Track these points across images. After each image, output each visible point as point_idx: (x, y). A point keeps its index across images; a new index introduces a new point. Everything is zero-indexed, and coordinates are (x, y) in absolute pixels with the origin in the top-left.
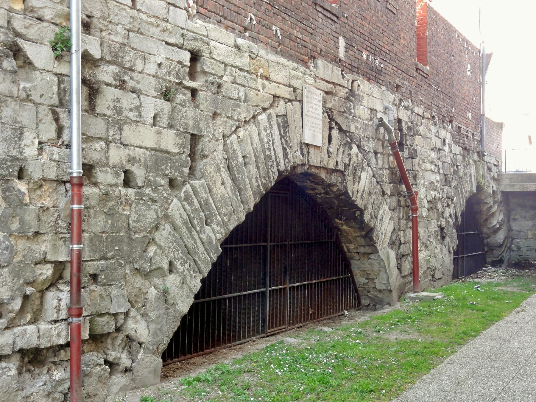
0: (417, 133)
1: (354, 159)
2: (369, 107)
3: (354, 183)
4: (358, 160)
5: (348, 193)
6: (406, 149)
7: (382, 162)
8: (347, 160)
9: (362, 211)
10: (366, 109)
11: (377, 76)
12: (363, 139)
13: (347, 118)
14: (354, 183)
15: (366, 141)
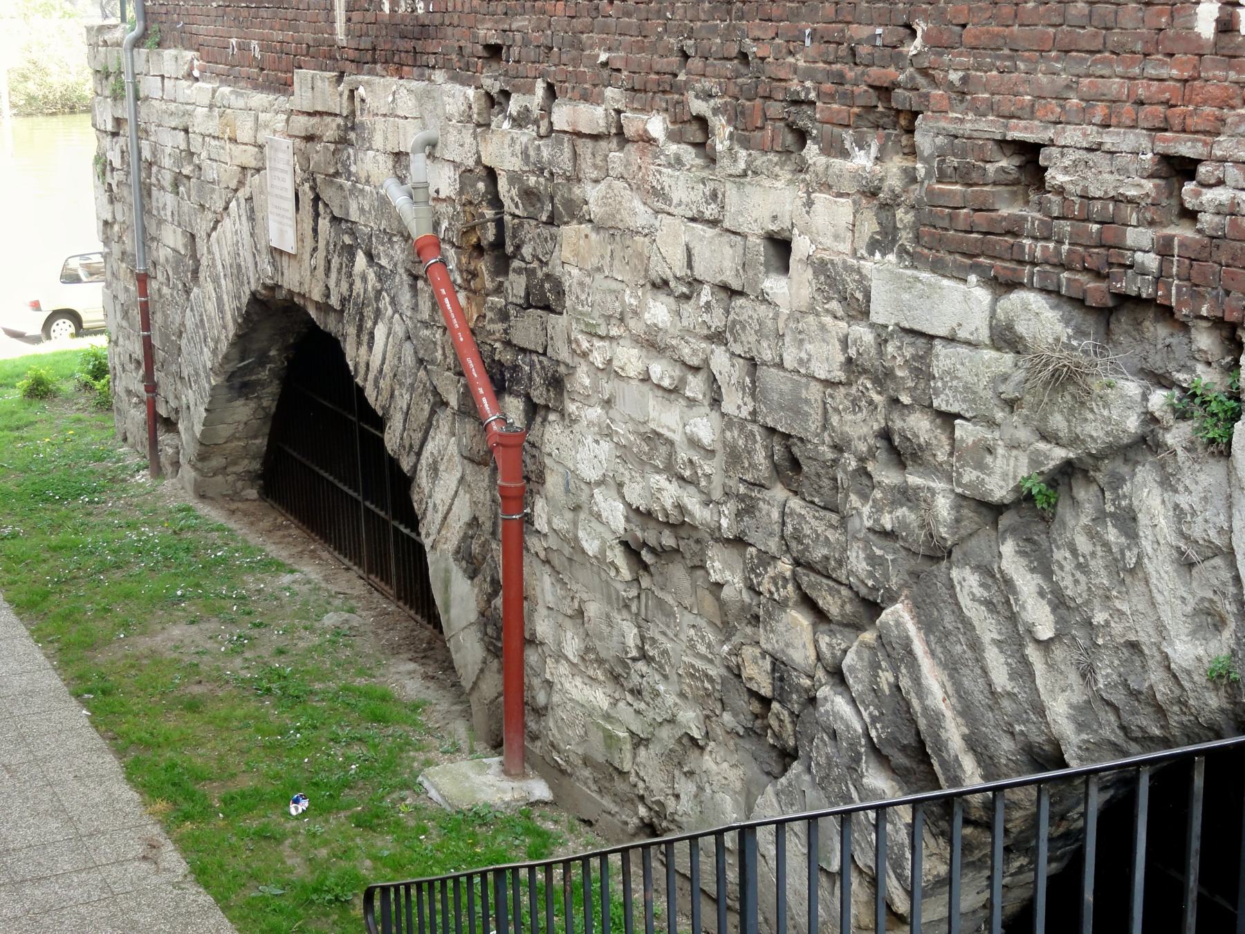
0: (574, 211)
1: (358, 286)
2: (389, 149)
3: (359, 344)
4: (365, 290)
5: (347, 365)
6: (519, 271)
7: (429, 304)
8: (344, 286)
9: (380, 423)
10: (381, 158)
11: (420, 45)
12: (378, 237)
13: (341, 187)
14: (359, 344)
15: (383, 244)
